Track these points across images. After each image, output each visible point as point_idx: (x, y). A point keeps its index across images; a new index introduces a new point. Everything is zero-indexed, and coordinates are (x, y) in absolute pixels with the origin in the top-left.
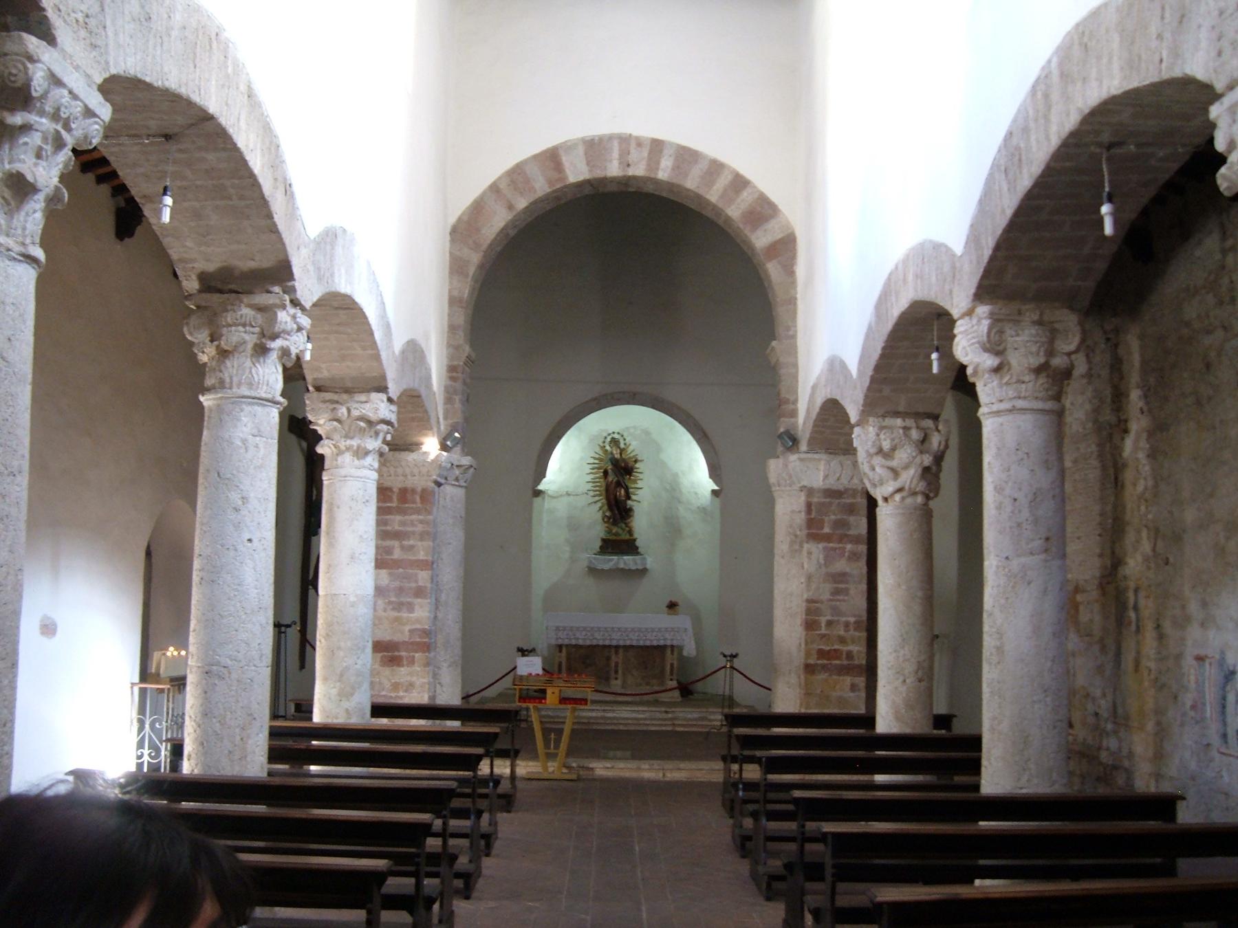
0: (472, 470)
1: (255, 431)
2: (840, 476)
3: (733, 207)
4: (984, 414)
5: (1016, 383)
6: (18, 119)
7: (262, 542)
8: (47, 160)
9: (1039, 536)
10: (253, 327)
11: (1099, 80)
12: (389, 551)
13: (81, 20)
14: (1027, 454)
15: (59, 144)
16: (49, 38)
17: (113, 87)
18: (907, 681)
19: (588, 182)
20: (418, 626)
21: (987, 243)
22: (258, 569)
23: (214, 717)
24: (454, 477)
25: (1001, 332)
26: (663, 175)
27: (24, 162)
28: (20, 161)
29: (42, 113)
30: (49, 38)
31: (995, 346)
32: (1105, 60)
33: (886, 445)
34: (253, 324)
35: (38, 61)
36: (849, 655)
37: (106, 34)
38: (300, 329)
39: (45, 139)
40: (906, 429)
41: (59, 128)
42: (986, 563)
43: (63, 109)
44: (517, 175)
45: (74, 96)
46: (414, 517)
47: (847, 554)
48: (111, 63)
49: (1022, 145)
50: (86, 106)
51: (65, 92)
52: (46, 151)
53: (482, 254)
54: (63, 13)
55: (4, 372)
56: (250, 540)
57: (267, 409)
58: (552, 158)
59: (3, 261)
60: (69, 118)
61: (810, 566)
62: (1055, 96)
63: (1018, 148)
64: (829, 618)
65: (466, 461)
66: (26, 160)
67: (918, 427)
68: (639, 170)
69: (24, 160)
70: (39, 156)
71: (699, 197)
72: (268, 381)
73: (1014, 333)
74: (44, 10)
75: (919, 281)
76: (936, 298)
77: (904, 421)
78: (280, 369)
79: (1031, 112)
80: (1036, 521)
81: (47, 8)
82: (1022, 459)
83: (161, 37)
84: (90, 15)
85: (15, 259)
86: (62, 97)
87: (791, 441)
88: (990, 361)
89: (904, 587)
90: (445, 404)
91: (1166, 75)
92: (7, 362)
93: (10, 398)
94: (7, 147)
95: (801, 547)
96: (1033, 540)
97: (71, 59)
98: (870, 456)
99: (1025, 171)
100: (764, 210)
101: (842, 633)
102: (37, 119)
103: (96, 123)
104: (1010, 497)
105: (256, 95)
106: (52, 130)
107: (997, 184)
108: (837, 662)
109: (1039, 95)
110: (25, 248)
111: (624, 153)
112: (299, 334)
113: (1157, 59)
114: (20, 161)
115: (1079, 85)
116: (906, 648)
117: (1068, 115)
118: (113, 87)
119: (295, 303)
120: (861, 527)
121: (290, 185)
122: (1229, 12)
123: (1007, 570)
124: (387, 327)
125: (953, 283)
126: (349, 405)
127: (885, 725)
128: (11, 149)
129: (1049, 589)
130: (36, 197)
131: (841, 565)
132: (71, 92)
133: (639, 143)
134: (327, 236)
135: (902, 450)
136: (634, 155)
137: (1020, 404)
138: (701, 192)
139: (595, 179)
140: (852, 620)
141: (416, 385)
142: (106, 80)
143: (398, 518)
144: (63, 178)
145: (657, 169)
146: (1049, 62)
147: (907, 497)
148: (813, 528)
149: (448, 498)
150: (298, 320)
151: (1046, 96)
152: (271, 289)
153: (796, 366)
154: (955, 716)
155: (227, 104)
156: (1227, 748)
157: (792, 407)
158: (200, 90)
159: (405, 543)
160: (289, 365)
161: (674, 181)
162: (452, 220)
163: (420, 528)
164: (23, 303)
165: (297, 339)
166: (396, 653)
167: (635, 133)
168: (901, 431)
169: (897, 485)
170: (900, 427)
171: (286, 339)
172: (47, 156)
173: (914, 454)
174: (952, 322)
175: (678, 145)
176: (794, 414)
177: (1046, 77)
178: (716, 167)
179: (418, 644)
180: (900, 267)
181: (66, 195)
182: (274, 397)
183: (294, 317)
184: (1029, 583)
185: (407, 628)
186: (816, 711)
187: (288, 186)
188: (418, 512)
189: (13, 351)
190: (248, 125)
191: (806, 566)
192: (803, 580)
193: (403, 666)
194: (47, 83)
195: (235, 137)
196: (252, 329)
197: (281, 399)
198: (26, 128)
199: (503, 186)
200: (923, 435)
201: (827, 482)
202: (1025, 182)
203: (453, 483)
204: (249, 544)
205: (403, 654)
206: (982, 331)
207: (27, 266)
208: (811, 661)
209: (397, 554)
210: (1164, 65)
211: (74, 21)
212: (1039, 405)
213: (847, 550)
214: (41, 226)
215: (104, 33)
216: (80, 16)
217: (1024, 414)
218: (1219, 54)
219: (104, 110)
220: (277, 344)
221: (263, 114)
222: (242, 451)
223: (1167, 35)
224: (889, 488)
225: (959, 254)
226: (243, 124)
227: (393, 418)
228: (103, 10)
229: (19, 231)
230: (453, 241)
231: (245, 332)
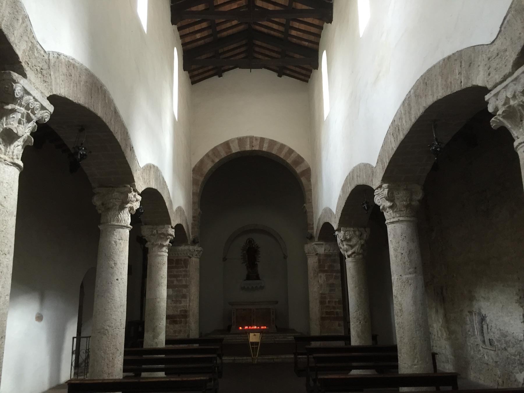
0: (202, 252)
1: (120, 238)
2: (330, 249)
3: (289, 159)
4: (387, 223)
5: (399, 211)
6: (10, 107)
7: (122, 280)
8: (23, 124)
9: (412, 267)
10: (119, 199)
11: (433, 95)
12: (173, 282)
13: (39, 70)
14: (405, 237)
15: (29, 120)
16: (24, 76)
17: (53, 99)
18: (361, 323)
19: (238, 152)
20: (183, 309)
21: (386, 162)
22: (120, 290)
23: (102, 350)
24: (195, 255)
25: (392, 193)
26: (264, 149)
27: (13, 125)
28: (11, 124)
29: (21, 105)
30: (24, 76)
31: (390, 198)
32: (435, 87)
33: (348, 237)
34: (119, 198)
35: (18, 83)
36: (337, 313)
37: (51, 77)
38: (137, 200)
39: (22, 116)
40: (354, 231)
41: (29, 112)
42: (392, 278)
43: (30, 104)
44: (215, 150)
45: (36, 100)
46: (181, 269)
47: (334, 277)
48: (54, 89)
49: (400, 124)
50: (41, 105)
51: (32, 98)
52: (23, 121)
53: (203, 177)
54: (30, 65)
55: (1, 211)
56: (117, 280)
57: (125, 230)
58: (227, 145)
59: (2, 165)
60: (33, 108)
61: (321, 281)
62: (413, 104)
63: (398, 126)
64: (329, 300)
65: (199, 249)
66: (14, 124)
67: (358, 231)
68: (257, 148)
69: (13, 124)
70: (19, 123)
71: (277, 156)
72: (125, 219)
73: (397, 193)
74: (21, 62)
75: (359, 178)
76: (366, 183)
77: (354, 228)
78: (130, 215)
79: (403, 112)
80: (411, 262)
81: (22, 62)
82: (404, 239)
83: (76, 83)
84: (43, 68)
85: (8, 164)
86: (30, 99)
87: (311, 238)
88: (388, 204)
89: (357, 288)
90: (192, 229)
91: (463, 87)
92: (4, 207)
93: (4, 222)
94: (5, 118)
95: (318, 275)
96: (410, 268)
97: (34, 84)
98: (342, 241)
99: (401, 133)
100: (299, 160)
101: (334, 305)
102: (19, 107)
103: (46, 112)
104: (400, 253)
105: (118, 113)
106: (26, 113)
107: (389, 140)
108: (333, 316)
109: (406, 105)
110: (13, 160)
111: (251, 142)
112: (137, 202)
113: (459, 82)
114: (11, 124)
115: (424, 98)
116: (360, 310)
117: (419, 110)
118: (53, 99)
119: (135, 191)
120: (338, 266)
121: (132, 147)
122: (493, 57)
123: (401, 280)
124: (171, 202)
125: (373, 177)
126: (157, 229)
127: (355, 341)
128: (6, 119)
129: (418, 287)
130: (19, 140)
131: (331, 281)
132: (34, 98)
133: (256, 139)
134: (147, 167)
135: (354, 239)
136: (255, 143)
137: (401, 219)
138: (278, 155)
139: (241, 151)
140: (337, 300)
141: (181, 223)
142: (50, 96)
143: (176, 270)
144: (32, 134)
145: (263, 148)
146: (410, 92)
147: (356, 255)
148: (321, 268)
149: (193, 262)
150: (136, 197)
151: (409, 105)
152: (126, 185)
153: (312, 212)
154: (437, 354)
155: (106, 114)
156: (486, 346)
157: (311, 226)
158: (94, 106)
159: (178, 279)
160: (133, 213)
161: (269, 151)
162: (193, 166)
163: (184, 273)
164: (12, 182)
165: (136, 204)
166: (175, 319)
167: (255, 136)
168: (353, 232)
169: (353, 250)
170: (352, 231)
171: (132, 204)
172: (23, 123)
173: (358, 240)
174: (373, 191)
175: (270, 139)
176: (313, 228)
177: (409, 98)
178: (283, 146)
179: (182, 315)
180: (351, 173)
181: (33, 140)
182: (127, 225)
183: (135, 196)
184: (410, 285)
185: (179, 310)
186: (326, 334)
187: (132, 148)
188: (183, 267)
189: (7, 202)
190: (115, 123)
191: (320, 281)
192: (318, 287)
193: (177, 324)
194: (22, 92)
195: (109, 126)
196: (119, 200)
197: (130, 226)
198: (13, 111)
199: (210, 154)
200: (360, 233)
201: (325, 252)
202: (401, 137)
203: (195, 257)
204: (117, 281)
205: (178, 319)
206: (385, 193)
207: (14, 167)
208: (324, 316)
209: (175, 283)
210: (462, 84)
211: (36, 70)
212: (409, 219)
213: (334, 275)
214: (22, 152)
215: (50, 77)
216: (38, 69)
217: (403, 222)
218: (489, 74)
219: (50, 108)
220: (129, 205)
221: (121, 120)
222: (115, 246)
223: (464, 72)
224: (350, 253)
225: (375, 167)
226: (112, 122)
227: (174, 234)
228: (49, 68)
229: (11, 153)
230: (193, 173)
231: (116, 201)
